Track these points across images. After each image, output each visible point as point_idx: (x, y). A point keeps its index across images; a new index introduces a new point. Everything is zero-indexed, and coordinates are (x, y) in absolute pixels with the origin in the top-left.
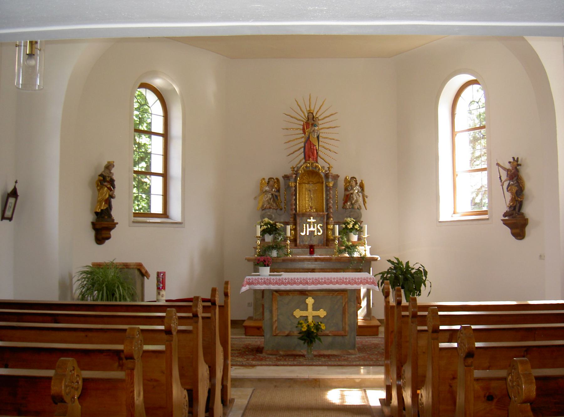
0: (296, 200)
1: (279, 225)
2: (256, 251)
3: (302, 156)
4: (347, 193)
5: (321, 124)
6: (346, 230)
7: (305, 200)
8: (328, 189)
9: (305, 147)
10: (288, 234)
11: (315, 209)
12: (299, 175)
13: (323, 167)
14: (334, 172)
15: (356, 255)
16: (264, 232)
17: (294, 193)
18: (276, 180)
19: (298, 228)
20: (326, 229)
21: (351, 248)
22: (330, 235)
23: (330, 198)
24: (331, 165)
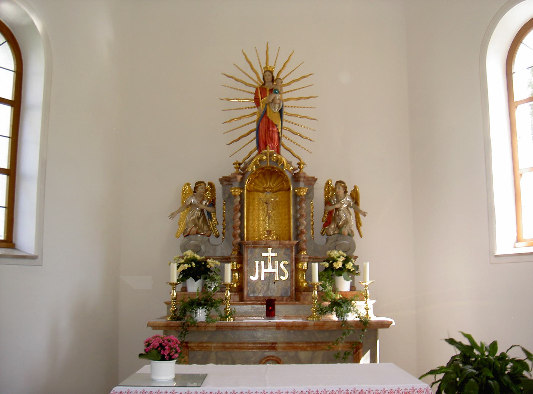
0: (242, 218)
1: (212, 263)
2: (168, 308)
3: (254, 144)
4: (330, 208)
5: (287, 93)
6: (330, 272)
7: (260, 220)
8: (298, 200)
9: (258, 130)
10: (228, 279)
11: (276, 234)
12: (248, 175)
13: (290, 163)
14: (308, 171)
15: (351, 317)
16: (185, 275)
17: (239, 207)
18: (208, 186)
19: (246, 268)
20: (295, 271)
21: (341, 304)
22: (302, 280)
23: (302, 216)
24: (303, 160)
